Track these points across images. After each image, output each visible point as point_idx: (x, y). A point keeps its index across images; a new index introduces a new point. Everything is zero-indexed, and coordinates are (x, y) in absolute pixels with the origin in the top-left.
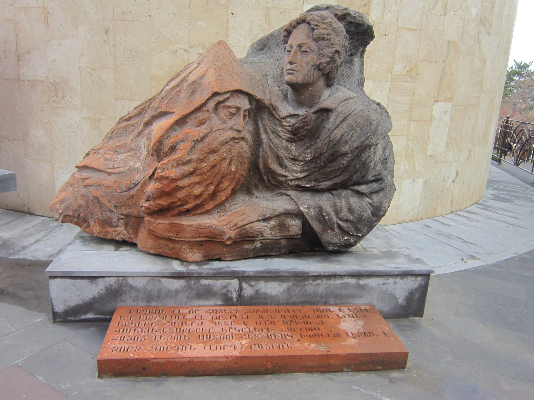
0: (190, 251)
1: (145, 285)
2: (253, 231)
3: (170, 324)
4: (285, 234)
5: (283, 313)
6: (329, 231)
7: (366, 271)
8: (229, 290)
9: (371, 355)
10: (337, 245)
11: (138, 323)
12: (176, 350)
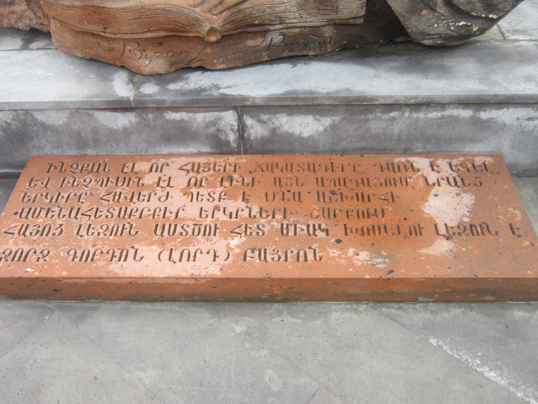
0: (142, 54)
1: (65, 121)
2: (261, 14)
3: (111, 196)
4: (330, 17)
5: (321, 174)
6: (424, 12)
7: (496, 96)
8: (221, 129)
9: (476, 280)
10: (442, 36)
11: (57, 194)
12: (107, 259)
